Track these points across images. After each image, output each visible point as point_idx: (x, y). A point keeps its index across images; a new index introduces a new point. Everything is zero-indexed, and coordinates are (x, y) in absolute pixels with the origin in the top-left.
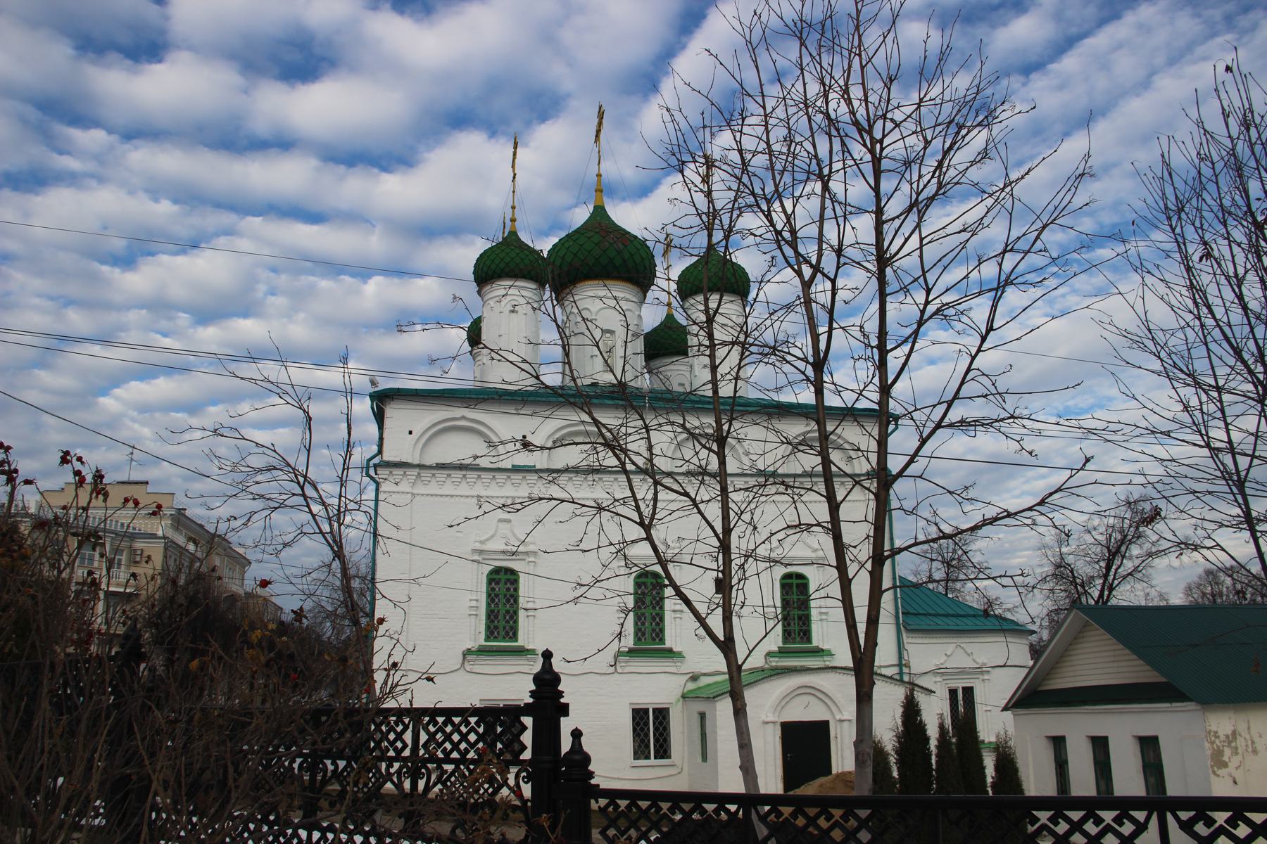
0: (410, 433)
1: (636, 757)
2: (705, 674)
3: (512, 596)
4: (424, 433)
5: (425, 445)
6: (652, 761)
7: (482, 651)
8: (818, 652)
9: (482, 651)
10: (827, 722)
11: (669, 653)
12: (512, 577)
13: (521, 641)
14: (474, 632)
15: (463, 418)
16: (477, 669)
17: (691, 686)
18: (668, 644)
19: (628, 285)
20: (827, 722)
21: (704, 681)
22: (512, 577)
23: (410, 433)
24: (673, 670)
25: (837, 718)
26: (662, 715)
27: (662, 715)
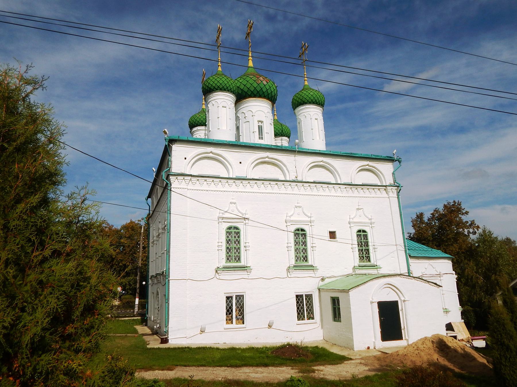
0: (185, 159)
1: (299, 319)
2: (327, 278)
3: (237, 240)
4: (194, 158)
5: (196, 161)
6: (306, 321)
7: (226, 268)
8: (374, 266)
9: (226, 268)
10: (397, 302)
11: (312, 268)
12: (237, 231)
13: (310, 263)
14: (290, 258)
15: (211, 152)
16: (222, 277)
17: (321, 283)
18: (310, 263)
19: (268, 101)
20: (397, 302)
21: (327, 281)
22: (237, 231)
23: (185, 159)
24: (313, 275)
25: (403, 299)
26: (309, 297)
27: (309, 297)
